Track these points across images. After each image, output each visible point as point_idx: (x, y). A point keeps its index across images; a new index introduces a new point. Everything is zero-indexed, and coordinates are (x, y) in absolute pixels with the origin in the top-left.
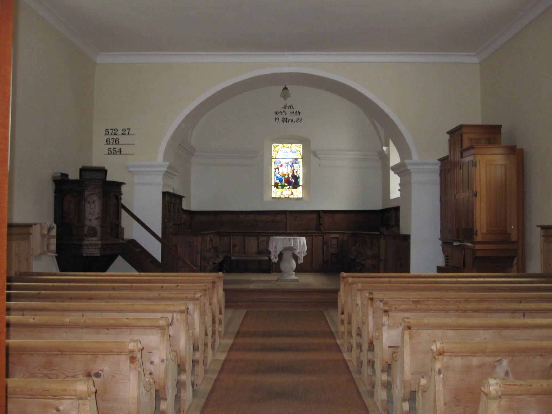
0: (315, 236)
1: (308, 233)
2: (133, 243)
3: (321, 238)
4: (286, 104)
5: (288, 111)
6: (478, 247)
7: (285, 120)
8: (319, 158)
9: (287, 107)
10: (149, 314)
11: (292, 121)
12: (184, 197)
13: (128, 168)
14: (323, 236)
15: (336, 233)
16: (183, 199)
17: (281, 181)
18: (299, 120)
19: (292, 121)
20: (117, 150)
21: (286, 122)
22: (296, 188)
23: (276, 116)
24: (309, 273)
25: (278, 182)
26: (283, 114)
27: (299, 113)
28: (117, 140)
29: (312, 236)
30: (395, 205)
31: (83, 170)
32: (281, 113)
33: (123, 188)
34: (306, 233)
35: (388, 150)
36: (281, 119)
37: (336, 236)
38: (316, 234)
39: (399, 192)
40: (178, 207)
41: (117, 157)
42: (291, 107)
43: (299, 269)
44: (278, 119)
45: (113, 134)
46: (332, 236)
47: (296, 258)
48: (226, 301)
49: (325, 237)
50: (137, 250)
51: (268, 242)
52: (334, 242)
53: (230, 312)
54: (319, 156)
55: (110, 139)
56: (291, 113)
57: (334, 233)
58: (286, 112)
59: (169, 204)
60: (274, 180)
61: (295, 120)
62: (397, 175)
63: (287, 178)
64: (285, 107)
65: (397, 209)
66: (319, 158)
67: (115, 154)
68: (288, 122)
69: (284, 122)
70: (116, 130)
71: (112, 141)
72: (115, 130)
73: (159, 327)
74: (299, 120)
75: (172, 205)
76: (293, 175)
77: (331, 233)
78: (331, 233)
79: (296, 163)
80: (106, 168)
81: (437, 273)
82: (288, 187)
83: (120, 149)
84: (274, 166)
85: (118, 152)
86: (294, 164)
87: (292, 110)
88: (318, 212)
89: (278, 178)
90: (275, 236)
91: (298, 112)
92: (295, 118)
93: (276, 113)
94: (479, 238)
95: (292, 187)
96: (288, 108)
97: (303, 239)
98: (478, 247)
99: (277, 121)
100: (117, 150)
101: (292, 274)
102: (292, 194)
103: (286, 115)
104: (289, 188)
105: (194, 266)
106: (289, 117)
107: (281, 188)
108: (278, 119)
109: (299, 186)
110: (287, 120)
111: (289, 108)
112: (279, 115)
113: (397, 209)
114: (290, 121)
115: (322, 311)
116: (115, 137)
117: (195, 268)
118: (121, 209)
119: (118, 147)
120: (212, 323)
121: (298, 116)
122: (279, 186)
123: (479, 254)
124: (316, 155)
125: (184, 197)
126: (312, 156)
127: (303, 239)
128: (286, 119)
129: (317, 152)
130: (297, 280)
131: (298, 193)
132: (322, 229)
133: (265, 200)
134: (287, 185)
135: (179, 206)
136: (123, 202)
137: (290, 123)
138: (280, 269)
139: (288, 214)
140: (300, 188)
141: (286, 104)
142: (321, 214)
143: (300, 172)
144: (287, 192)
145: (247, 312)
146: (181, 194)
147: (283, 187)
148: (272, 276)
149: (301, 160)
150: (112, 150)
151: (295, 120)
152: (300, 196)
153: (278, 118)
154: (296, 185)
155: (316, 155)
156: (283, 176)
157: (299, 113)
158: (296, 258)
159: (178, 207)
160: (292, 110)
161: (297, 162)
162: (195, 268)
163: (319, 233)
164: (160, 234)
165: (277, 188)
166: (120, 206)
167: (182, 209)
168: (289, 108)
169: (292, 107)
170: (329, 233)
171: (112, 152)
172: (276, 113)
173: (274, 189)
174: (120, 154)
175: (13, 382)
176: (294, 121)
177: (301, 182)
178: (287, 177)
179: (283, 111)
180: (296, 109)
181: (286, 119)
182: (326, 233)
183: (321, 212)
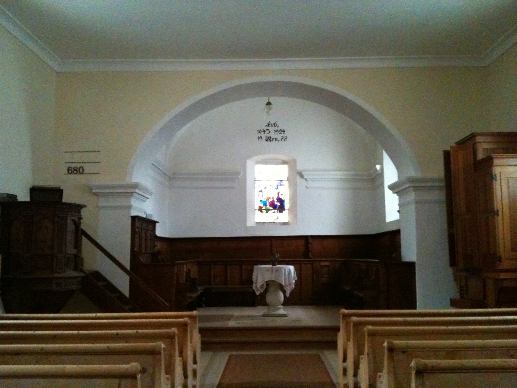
0: (304, 264)
1: (296, 261)
2: (97, 275)
3: (309, 266)
4: (270, 122)
5: (272, 129)
6: (502, 276)
7: (269, 139)
8: (306, 179)
9: (271, 125)
11: (276, 139)
12: (158, 222)
13: (92, 190)
14: (312, 264)
15: (326, 261)
16: (157, 225)
17: (265, 204)
18: (284, 139)
19: (276, 139)
21: (270, 141)
22: (282, 212)
23: (260, 135)
24: (298, 306)
25: (262, 206)
26: (267, 132)
27: (284, 131)
29: (300, 264)
30: (394, 228)
31: (34, 190)
32: (264, 131)
33: (84, 212)
34: (294, 261)
35: (382, 169)
36: (264, 138)
37: (327, 263)
38: (304, 263)
39: (398, 214)
40: (150, 233)
41: (78, 177)
42: (275, 125)
43: (288, 302)
44: (261, 137)
46: (323, 263)
47: (284, 292)
48: (203, 343)
49: (314, 264)
50: (100, 284)
51: (252, 271)
52: (325, 270)
53: (209, 354)
54: (305, 177)
56: (276, 131)
57: (324, 261)
58: (270, 130)
59: (146, 232)
60: (258, 204)
61: (279, 139)
62: (395, 195)
63: (272, 201)
64: (268, 125)
65: (397, 233)
66: (306, 179)
68: (271, 142)
69: (267, 141)
74: (284, 139)
75: (143, 231)
76: (278, 198)
77: (322, 261)
78: (322, 261)
79: (281, 185)
80: (61, 188)
82: (273, 211)
84: (257, 189)
86: (279, 186)
87: (276, 128)
88: (306, 238)
89: (262, 202)
90: (260, 265)
91: (282, 130)
92: (279, 136)
93: (260, 132)
94: (506, 264)
95: (277, 211)
96: (272, 126)
97: (292, 268)
98: (502, 276)
99: (260, 140)
101: (280, 308)
102: (278, 218)
103: (269, 134)
104: (274, 212)
105: (166, 301)
106: (273, 135)
107: (266, 212)
108: (261, 137)
109: (284, 209)
110: (271, 139)
111: (273, 125)
112: (262, 134)
113: (397, 233)
114: (274, 140)
115: (319, 355)
117: (168, 305)
118: (81, 237)
120: (183, 378)
121: (282, 135)
122: (263, 210)
123: (505, 284)
124: (302, 176)
125: (158, 222)
126: (298, 177)
127: (292, 268)
128: (269, 138)
129: (304, 173)
130: (285, 315)
131: (284, 217)
132: (310, 256)
134: (272, 208)
135: (151, 232)
136: (83, 227)
137: (274, 143)
138: (265, 301)
139: (273, 239)
140: (286, 213)
141: (270, 122)
142: (310, 240)
143: (286, 197)
144: (272, 216)
145: (230, 357)
146: (155, 219)
147: (267, 210)
148: (259, 311)
149: (287, 181)
151: (279, 139)
152: (286, 221)
153: (261, 137)
154: (281, 208)
155: (302, 176)
156: (267, 200)
157: (284, 131)
158: (282, 288)
160: (276, 128)
161: (282, 184)
162: (168, 305)
163: (308, 261)
164: (128, 265)
165: (261, 212)
166: (80, 232)
167: (156, 236)
168: (273, 125)
169: (275, 125)
170: (319, 261)
172: (259, 131)
173: (258, 212)
176: (278, 140)
177: (287, 205)
178: (271, 200)
179: (267, 129)
180: (281, 127)
181: (269, 138)
182: (316, 261)
183: (309, 238)
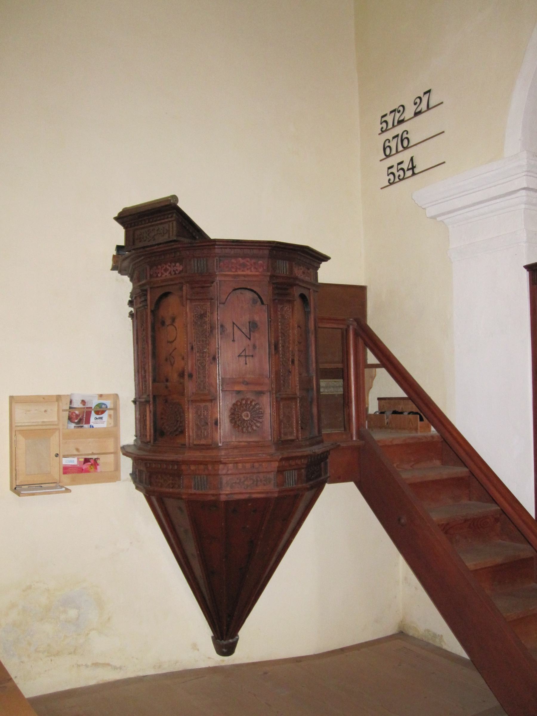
10: (220, 395)
20: (405, 166)
28: (405, 135)
45: (396, 123)
55: (391, 139)
67: (403, 179)
70: (401, 109)
71: (393, 144)
72: (399, 112)
73: (260, 422)
81: (385, 119)
83: (412, 159)
85: (408, 169)
100: (405, 166)
116: (399, 130)
119: (405, 156)
125: (326, 258)
133: (365, 369)
150: (394, 170)
159: (217, 270)
171: (397, 174)
174: (414, 174)
175: (343, 393)
